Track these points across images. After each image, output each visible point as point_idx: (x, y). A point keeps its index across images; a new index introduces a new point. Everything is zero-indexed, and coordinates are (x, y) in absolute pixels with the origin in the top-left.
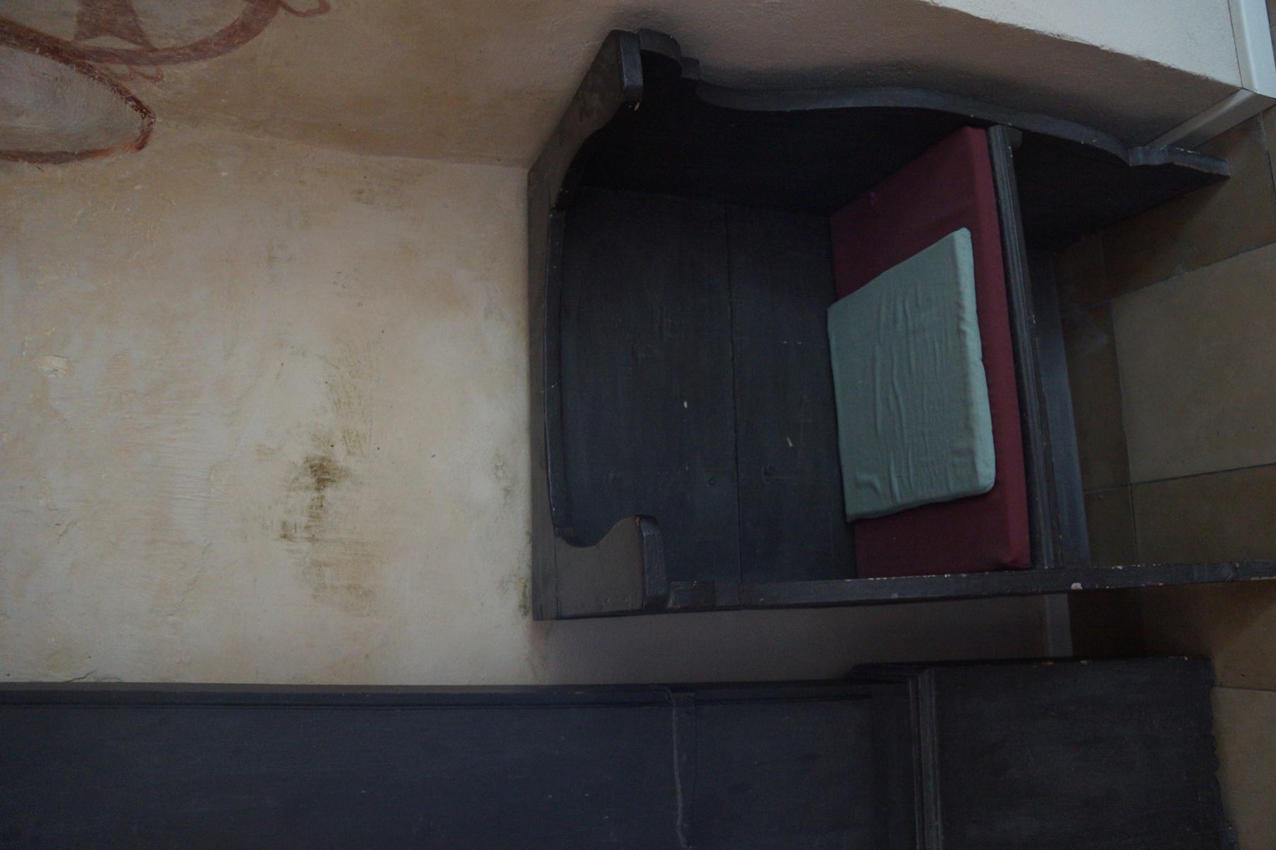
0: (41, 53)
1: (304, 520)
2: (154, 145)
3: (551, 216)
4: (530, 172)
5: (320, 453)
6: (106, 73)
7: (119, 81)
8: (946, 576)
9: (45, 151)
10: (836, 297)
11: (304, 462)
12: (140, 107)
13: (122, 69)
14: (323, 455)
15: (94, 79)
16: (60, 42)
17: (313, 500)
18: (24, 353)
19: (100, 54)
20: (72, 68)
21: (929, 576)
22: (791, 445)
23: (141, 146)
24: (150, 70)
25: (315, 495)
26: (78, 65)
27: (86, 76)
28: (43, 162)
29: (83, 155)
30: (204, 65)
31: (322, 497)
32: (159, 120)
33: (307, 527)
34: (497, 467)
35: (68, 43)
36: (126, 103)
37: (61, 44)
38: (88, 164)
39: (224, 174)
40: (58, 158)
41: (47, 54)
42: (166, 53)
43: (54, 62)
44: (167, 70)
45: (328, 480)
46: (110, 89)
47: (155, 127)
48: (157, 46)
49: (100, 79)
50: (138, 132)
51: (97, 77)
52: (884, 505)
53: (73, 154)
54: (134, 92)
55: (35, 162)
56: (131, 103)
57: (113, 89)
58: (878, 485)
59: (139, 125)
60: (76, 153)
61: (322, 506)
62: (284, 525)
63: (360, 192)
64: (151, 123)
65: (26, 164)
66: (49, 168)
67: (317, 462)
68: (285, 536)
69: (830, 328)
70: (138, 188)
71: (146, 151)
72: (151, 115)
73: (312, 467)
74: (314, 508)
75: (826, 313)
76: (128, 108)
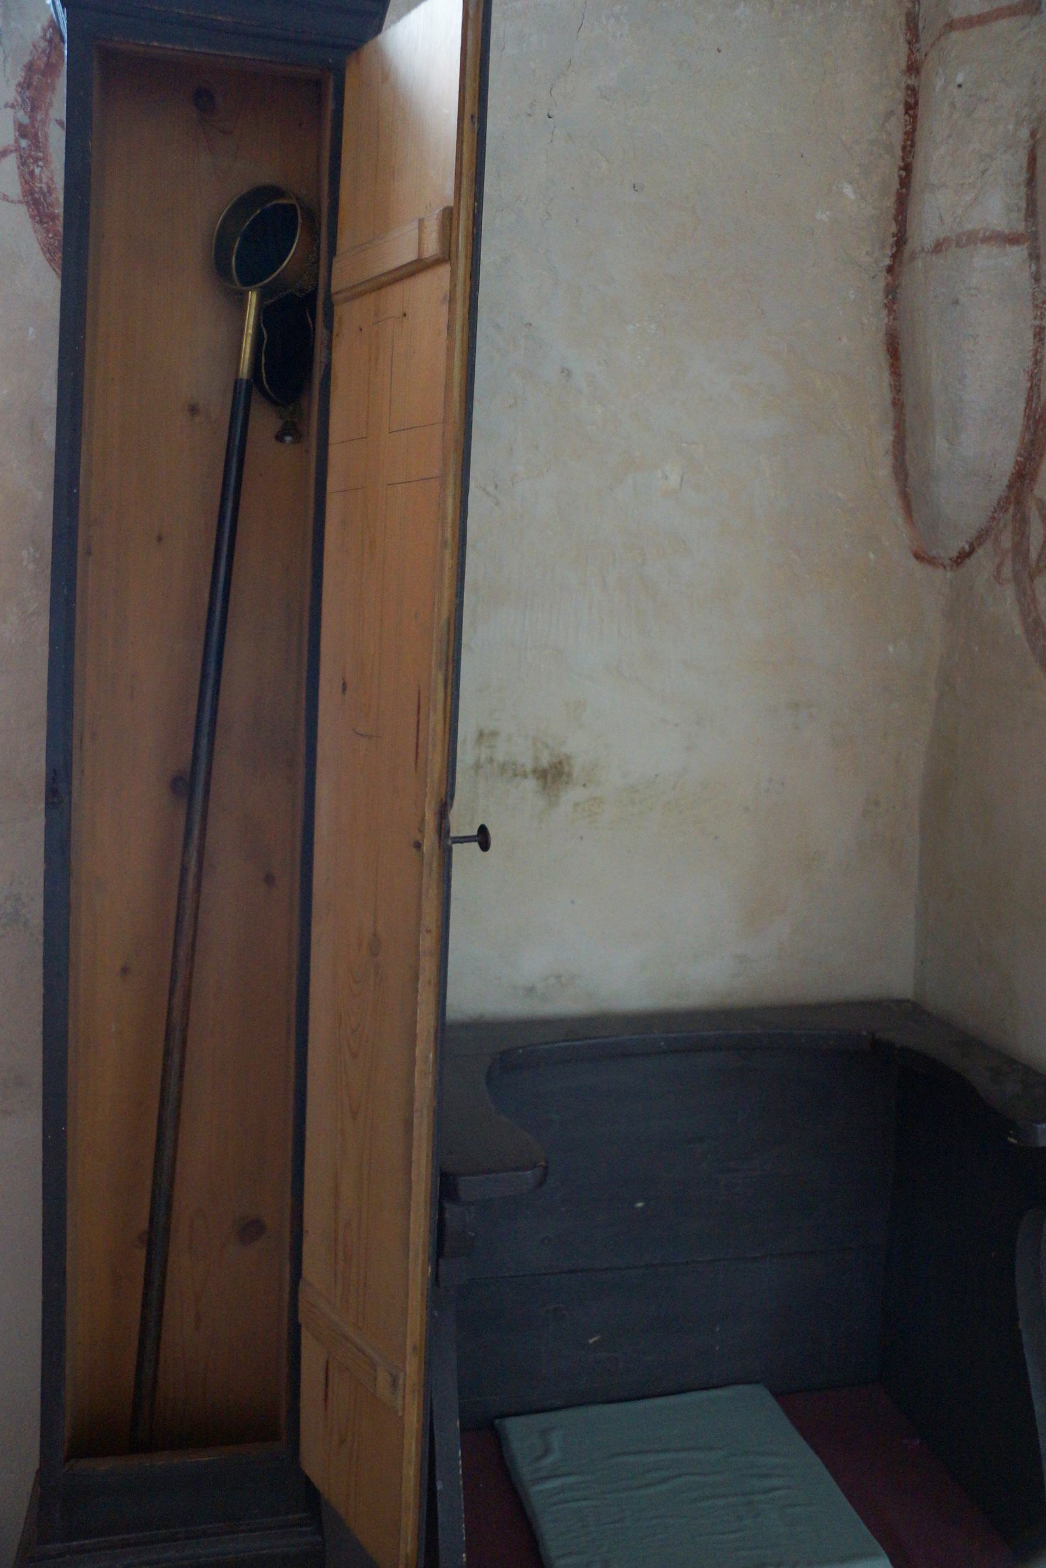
0: (1017, 462)
1: (500, 757)
2: (919, 570)
3: (864, 1033)
4: (908, 1001)
5: (576, 771)
6: (1001, 525)
7: (993, 537)
8: (464, 1555)
9: (907, 457)
10: (779, 1395)
11: (565, 755)
12: (962, 557)
13: (1007, 541)
14: (575, 776)
15: (993, 512)
16: (1032, 482)
17: (523, 765)
18: (684, 445)
19: (1022, 523)
20: (1003, 491)
21: (464, 1531)
22: (591, 1341)
23: (918, 556)
24: (1007, 571)
25: (529, 768)
26: (1007, 498)
27: (996, 505)
28: (895, 457)
29: (906, 499)
30: (1019, 631)
31: (525, 775)
32: (949, 575)
33: (491, 760)
34: (558, 977)
35: (1032, 490)
36: (967, 542)
37: (1030, 483)
38: (894, 501)
39: (891, 649)
40: (901, 470)
41: (1017, 468)
42: (1029, 592)
43: (1009, 474)
44: (1009, 591)
45: (546, 783)
46: (983, 528)
47: (941, 570)
48: (1035, 582)
49: (993, 518)
50: (934, 552)
51: (995, 515)
52: (524, 1468)
53: (906, 487)
54: (980, 551)
55: (894, 446)
56: (967, 547)
57: (983, 530)
58: (549, 1460)
59: (942, 555)
60: (907, 489)
61: (516, 775)
62: (494, 734)
63: (877, 804)
64: (945, 567)
65: (891, 438)
66: (888, 461)
67: (566, 769)
68: (481, 735)
69: (741, 1387)
70: (871, 556)
71: (913, 562)
72: (955, 568)
73: (560, 763)
74: (514, 767)
75: (757, 1382)
76: (964, 545)
